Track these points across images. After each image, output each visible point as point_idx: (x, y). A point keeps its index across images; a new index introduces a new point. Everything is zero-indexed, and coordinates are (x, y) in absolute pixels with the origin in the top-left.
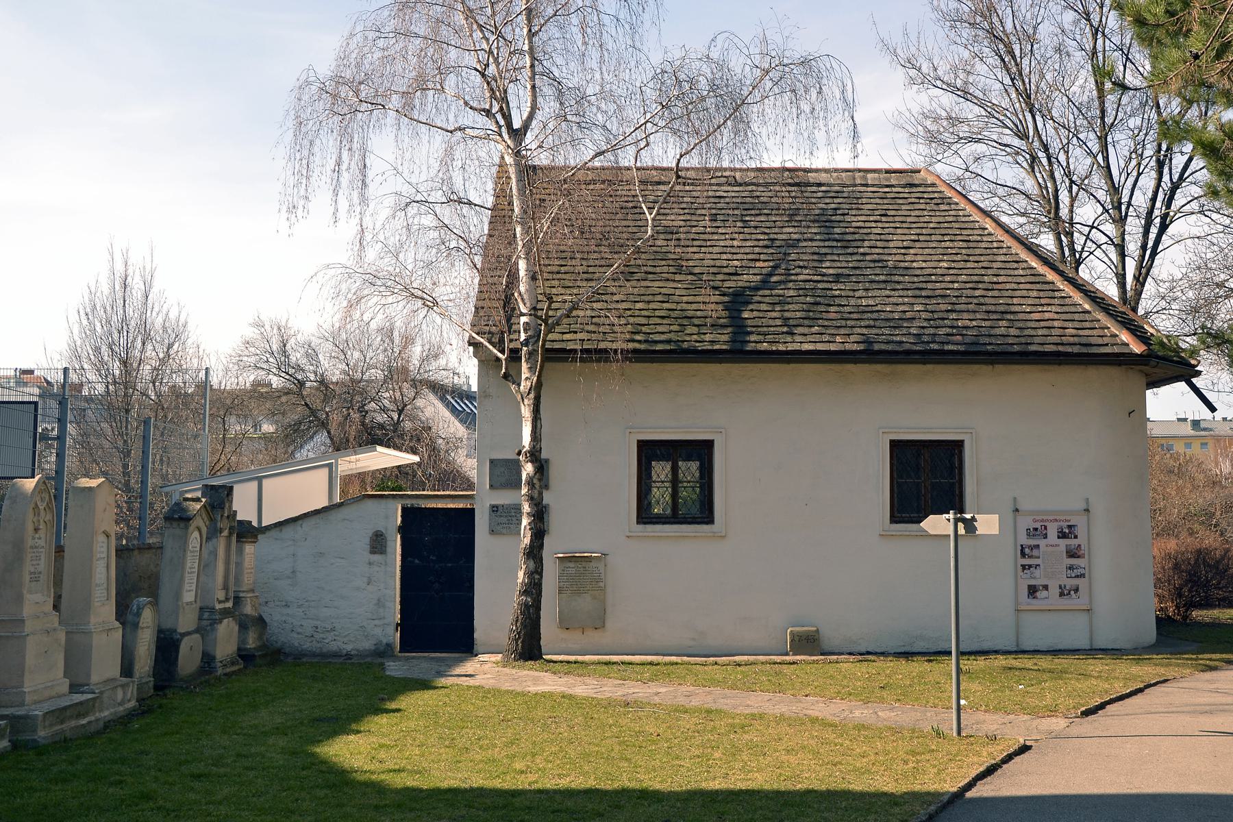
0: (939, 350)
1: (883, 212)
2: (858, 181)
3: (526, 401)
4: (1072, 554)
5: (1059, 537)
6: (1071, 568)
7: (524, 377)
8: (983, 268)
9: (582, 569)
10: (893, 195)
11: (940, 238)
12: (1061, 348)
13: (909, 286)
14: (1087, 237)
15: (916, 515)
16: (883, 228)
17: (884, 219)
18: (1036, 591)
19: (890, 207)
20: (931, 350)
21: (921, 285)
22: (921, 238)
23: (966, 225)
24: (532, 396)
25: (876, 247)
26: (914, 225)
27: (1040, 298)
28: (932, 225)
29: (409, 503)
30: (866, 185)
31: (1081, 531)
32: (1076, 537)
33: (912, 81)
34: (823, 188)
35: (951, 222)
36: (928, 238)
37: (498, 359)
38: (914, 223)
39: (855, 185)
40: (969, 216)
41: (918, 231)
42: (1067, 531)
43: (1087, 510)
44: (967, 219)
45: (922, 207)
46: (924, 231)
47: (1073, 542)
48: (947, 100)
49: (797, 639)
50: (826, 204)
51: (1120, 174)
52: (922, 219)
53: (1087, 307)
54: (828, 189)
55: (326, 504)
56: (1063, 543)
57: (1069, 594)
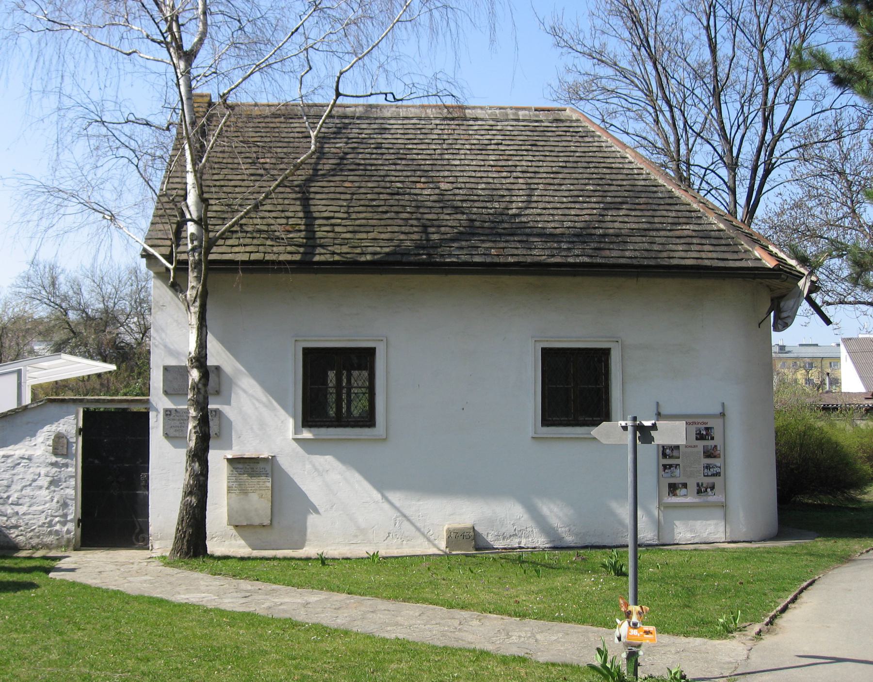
0: (589, 263)
1: (534, 143)
2: (511, 117)
3: (192, 309)
4: (710, 454)
5: (697, 439)
6: (708, 467)
7: (190, 285)
8: (625, 191)
9: (250, 470)
10: (542, 129)
11: (585, 165)
12: (699, 262)
13: (558, 205)
14: (703, 179)
15: (558, 419)
16: (534, 156)
17: (534, 148)
18: (677, 489)
19: (540, 138)
20: (580, 263)
21: (569, 205)
22: (568, 165)
23: (608, 155)
24: (197, 304)
25: (528, 172)
26: (562, 154)
27: (679, 217)
28: (577, 154)
29: (92, 407)
30: (518, 120)
31: (717, 433)
32: (712, 438)
33: (558, 45)
34: (480, 123)
35: (595, 152)
36: (575, 165)
37: (168, 270)
38: (562, 152)
39: (507, 120)
40: (611, 147)
41: (566, 159)
42: (704, 433)
43: (723, 415)
44: (609, 149)
45: (569, 139)
46: (571, 159)
47: (709, 443)
48: (587, 65)
49: (453, 535)
50: (482, 135)
51: (732, 127)
52: (568, 149)
53: (722, 226)
54: (484, 123)
55: (14, 405)
56: (701, 444)
57: (706, 491)
